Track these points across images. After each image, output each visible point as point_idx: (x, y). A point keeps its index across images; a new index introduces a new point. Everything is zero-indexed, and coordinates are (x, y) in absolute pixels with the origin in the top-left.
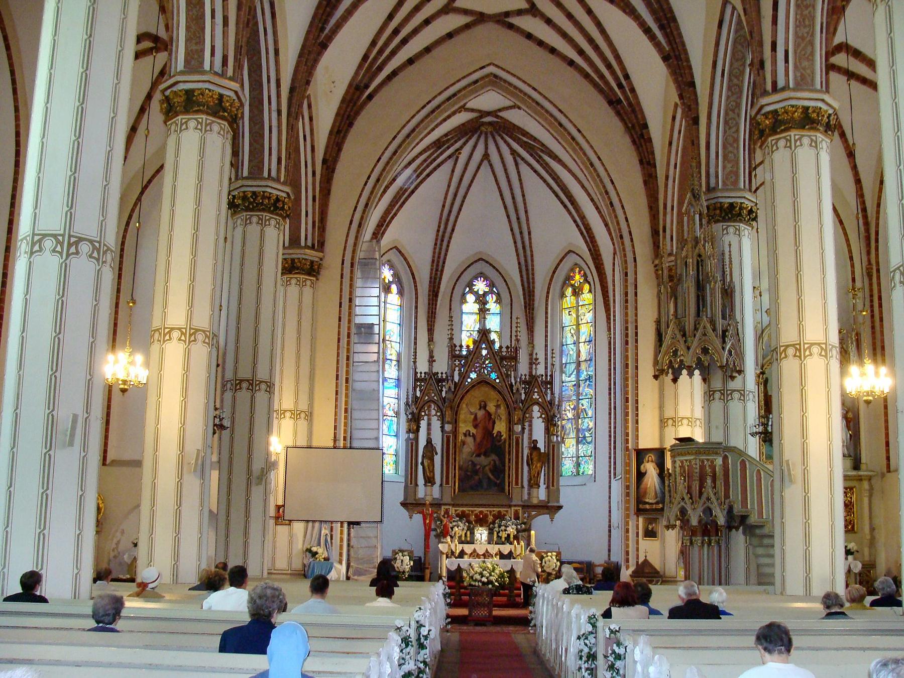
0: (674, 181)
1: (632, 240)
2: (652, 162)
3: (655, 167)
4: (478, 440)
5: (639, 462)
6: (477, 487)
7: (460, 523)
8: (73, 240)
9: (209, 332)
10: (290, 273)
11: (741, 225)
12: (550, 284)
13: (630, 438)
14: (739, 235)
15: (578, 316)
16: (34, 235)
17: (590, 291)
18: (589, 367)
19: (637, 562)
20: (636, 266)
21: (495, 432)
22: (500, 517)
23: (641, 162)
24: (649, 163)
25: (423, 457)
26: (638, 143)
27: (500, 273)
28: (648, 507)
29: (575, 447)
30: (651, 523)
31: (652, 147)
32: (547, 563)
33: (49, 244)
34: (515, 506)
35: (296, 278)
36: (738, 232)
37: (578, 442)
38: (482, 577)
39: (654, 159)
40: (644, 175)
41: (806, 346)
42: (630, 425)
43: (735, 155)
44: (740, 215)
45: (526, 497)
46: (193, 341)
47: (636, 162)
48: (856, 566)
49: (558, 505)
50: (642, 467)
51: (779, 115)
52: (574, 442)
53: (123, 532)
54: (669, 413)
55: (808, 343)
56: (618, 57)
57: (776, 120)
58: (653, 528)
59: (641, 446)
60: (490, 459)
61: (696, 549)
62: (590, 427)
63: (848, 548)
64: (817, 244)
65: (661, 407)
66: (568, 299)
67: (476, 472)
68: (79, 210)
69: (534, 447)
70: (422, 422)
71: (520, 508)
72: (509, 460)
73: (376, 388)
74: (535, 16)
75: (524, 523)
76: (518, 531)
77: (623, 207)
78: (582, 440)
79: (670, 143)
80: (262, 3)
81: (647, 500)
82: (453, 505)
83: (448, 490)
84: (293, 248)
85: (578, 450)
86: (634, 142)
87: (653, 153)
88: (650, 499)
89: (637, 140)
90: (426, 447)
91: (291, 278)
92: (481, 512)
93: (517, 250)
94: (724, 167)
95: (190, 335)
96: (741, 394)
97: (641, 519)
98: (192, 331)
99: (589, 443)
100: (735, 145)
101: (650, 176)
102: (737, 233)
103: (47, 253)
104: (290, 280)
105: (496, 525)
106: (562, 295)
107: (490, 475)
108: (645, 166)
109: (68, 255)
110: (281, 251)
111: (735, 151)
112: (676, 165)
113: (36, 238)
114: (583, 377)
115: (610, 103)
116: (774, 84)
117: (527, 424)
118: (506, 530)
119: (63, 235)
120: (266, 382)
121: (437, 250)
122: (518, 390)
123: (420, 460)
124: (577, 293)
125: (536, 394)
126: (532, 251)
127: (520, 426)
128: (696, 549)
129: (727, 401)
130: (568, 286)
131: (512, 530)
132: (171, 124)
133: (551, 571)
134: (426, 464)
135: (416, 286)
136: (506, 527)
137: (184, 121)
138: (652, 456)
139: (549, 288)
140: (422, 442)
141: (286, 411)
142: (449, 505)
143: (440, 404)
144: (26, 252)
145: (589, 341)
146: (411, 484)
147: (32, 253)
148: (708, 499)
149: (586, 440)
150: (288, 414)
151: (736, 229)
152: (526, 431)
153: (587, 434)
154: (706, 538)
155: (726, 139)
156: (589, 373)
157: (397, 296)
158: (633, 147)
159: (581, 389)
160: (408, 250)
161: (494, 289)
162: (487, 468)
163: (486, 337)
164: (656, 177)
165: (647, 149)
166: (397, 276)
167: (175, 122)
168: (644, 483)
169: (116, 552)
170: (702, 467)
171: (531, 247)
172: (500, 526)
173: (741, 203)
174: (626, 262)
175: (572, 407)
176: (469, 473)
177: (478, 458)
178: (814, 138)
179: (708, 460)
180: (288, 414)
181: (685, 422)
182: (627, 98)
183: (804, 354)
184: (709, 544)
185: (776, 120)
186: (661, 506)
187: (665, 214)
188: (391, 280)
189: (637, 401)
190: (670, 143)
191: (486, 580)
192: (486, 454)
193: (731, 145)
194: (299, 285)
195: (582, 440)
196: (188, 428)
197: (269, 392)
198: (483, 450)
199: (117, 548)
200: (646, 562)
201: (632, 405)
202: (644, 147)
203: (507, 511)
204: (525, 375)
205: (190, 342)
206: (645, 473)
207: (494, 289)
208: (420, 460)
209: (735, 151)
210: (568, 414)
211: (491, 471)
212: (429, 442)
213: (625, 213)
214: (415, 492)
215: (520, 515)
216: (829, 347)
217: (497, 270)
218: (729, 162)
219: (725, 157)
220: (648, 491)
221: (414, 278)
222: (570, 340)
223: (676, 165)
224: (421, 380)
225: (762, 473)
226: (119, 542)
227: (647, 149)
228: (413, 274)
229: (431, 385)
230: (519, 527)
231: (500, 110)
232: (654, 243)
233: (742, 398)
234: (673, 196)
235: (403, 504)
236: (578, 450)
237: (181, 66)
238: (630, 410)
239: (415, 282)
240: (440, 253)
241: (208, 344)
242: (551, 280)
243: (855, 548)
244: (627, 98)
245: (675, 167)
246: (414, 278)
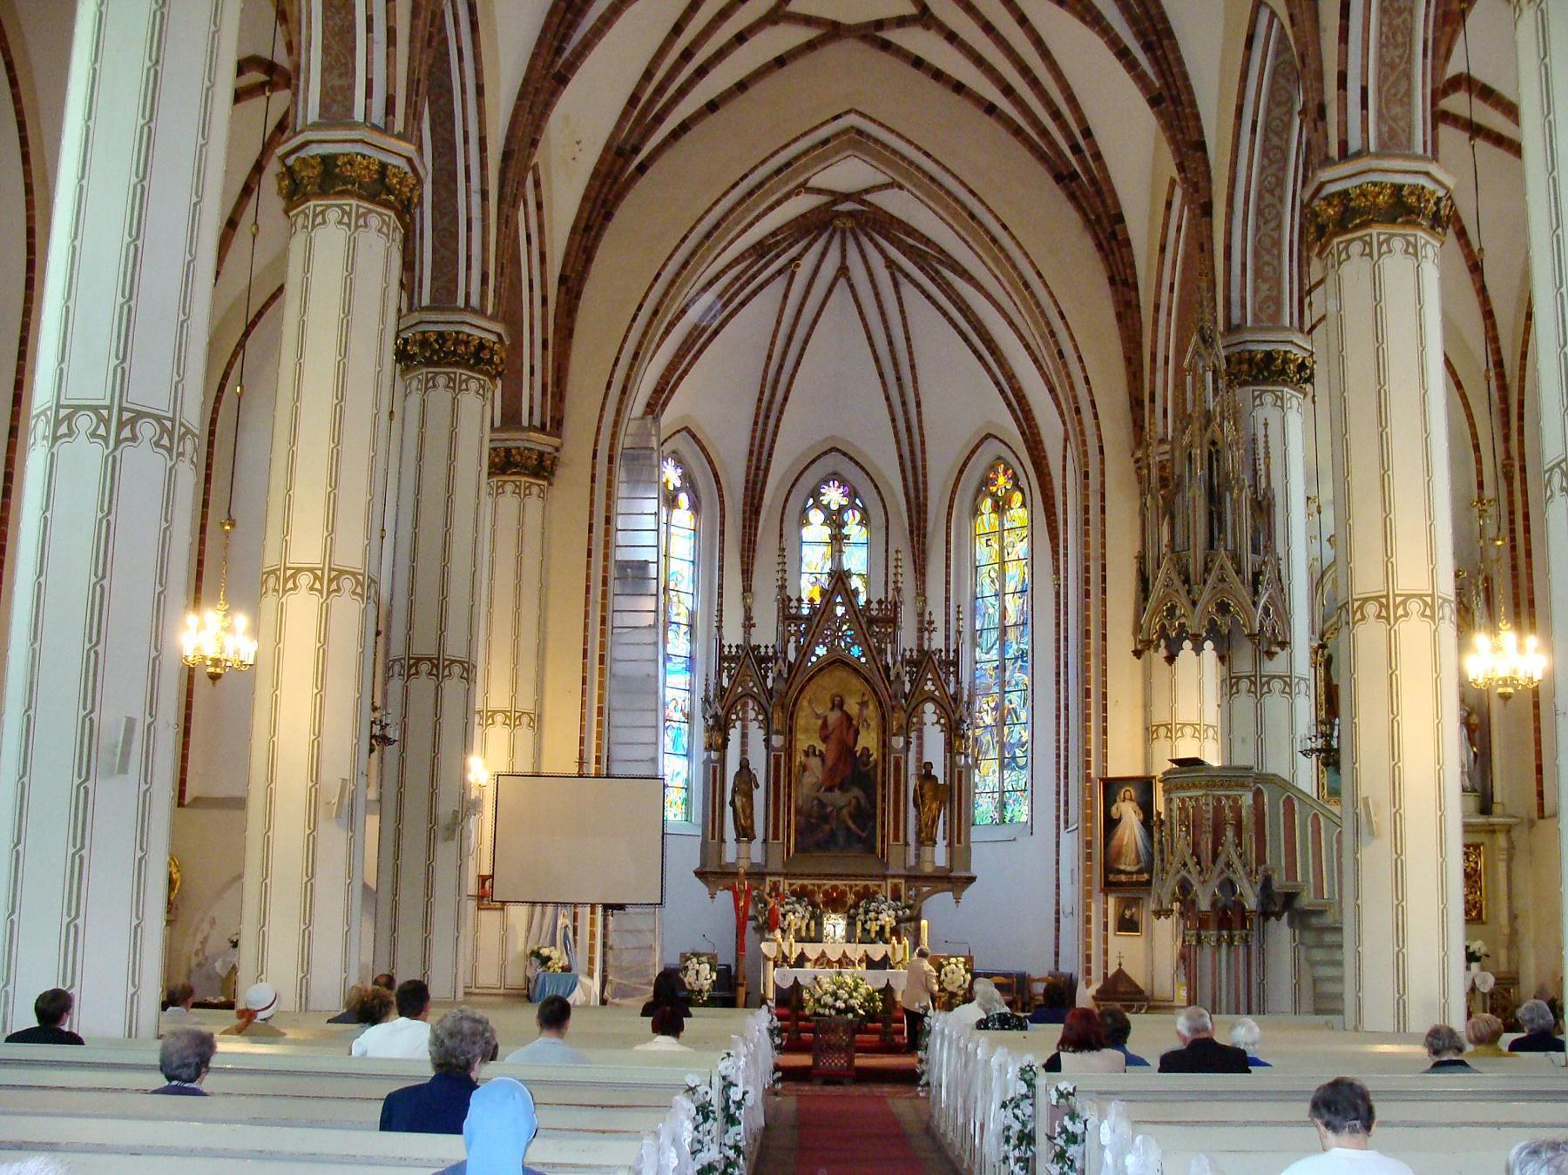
0: (1169, 314)
1: (1096, 416)
2: (1130, 281)
3: (1136, 289)
4: (829, 762)
5: (1109, 801)
6: (827, 844)
7: (797, 906)
8: (126, 415)
9: (363, 575)
10: (504, 473)
11: (1286, 389)
12: (954, 492)
13: (1093, 759)
14: (1282, 408)
15: (1002, 548)
16: (59, 406)
17: (1024, 505)
18: (1022, 636)
19: (1106, 974)
20: (1103, 462)
21: (858, 748)
22: (867, 895)
23: (1112, 280)
24: (1125, 283)
25: (734, 791)
26: (1106, 247)
27: (867, 474)
28: (1123, 878)
29: (997, 774)
30: (1129, 907)
31: (1131, 255)
32: (949, 975)
33: (84, 422)
34: (894, 876)
36: (1280, 403)
37: (1002, 767)
38: (836, 1000)
39: (1135, 275)
40: (1117, 303)
41: (1398, 600)
42: (1093, 736)
43: (1274, 269)
44: (1283, 372)
45: (912, 861)
46: (334, 591)
47: (1103, 280)
48: (1485, 981)
49: (967, 875)
50: (1114, 809)
51: (1351, 199)
52: (995, 765)
53: (213, 922)
54: (1160, 716)
55: (1401, 595)
56: (1071, 99)
57: (1346, 208)
58: (1132, 915)
59: (1112, 773)
60: (850, 795)
61: (1207, 951)
62: (1024, 740)
63: (1471, 950)
64: (1418, 423)
65: (1147, 706)
66: (985, 517)
68: (137, 364)
70: (732, 731)
71: (903, 881)
72: (884, 797)
73: (652, 673)
74: (927, 27)
75: (910, 907)
76: (899, 920)
77: (1080, 358)
78: (1009, 763)
79: (1163, 249)
80: (454, 6)
81: (1122, 867)
82: (786, 876)
83: (777, 848)
85: (1002, 780)
86: (1099, 246)
87: (1132, 265)
88: (1127, 864)
89: (1105, 243)
90: (738, 774)
91: (505, 482)
92: (834, 888)
93: (896, 434)
94: (1256, 290)
95: (330, 581)
96: (1285, 682)
97: (1111, 900)
98: (334, 574)
99: (1022, 768)
100: (1276, 252)
101: (1128, 304)
102: (1279, 403)
103: (82, 439)
105: (861, 910)
106: (976, 512)
107: (850, 823)
109: (118, 442)
110: (487, 436)
112: (1172, 285)
113: (63, 413)
114: (1011, 653)
115: (1059, 178)
116: (1343, 145)
117: (913, 735)
118: (877, 919)
119: (109, 408)
120: (461, 663)
121: (758, 434)
123: (728, 798)
124: (1000, 507)
125: (929, 683)
126: (922, 435)
127: (902, 739)
128: (1207, 951)
129: (1262, 695)
130: (986, 496)
131: (887, 919)
132: (297, 215)
133: (955, 990)
134: (739, 804)
135: (721, 496)
136: (878, 913)
137: (319, 209)
138: (1130, 791)
139: (952, 500)
140: (732, 767)
142: (779, 875)
143: (764, 701)
144: (44, 438)
145: (1022, 592)
146: (713, 838)
147: (55, 439)
148: (1229, 865)
149: (1017, 763)
151: (1277, 396)
152: (913, 747)
153: (1018, 753)
154: (1225, 933)
155: (1260, 240)
156: (1022, 646)
157: (689, 513)
158: (1098, 256)
159: (1008, 674)
160: (707, 434)
161: (858, 501)
162: (845, 811)
163: (844, 583)
164: (1138, 306)
165: (1122, 258)
166: (688, 479)
167: (303, 211)
168: (1117, 837)
169: (201, 957)
170: (1218, 810)
171: (921, 428)
172: (866, 912)
173: (1286, 352)
175: (992, 705)
176: (813, 820)
177: (829, 794)
178: (1412, 239)
179: (1227, 797)
181: (1188, 731)
182: (1087, 170)
183: (1395, 613)
185: (1346, 208)
186: (1146, 876)
187: (1153, 372)
188: (678, 485)
189: (1105, 696)
190: (1163, 249)
192: (843, 787)
193: (1269, 252)
194: (519, 494)
195: (1009, 763)
196: (327, 741)
197: (467, 680)
198: (838, 780)
199: (203, 949)
200: (1120, 973)
201: (1096, 702)
202: (1117, 254)
203: (879, 886)
204: (911, 650)
205: (329, 593)
206: (1120, 820)
207: (858, 501)
208: (728, 798)
209: (1276, 262)
210: (985, 717)
211: (851, 816)
212: (744, 765)
213: (1084, 369)
214: (720, 853)
215: (903, 893)
216: (1438, 602)
217: (862, 468)
218: (1265, 280)
219: (1258, 272)
220: (1124, 850)
221: (718, 482)
222: (988, 590)
223: (1172, 285)
224: (730, 659)
225: (1322, 819)
226: (206, 939)
227: (1122, 258)
228: (716, 475)
229: (748, 666)
230: (900, 913)
231: (867, 191)
232: (1135, 421)
233: (1287, 690)
234: (1168, 340)
235: (700, 874)
236: (1002, 780)
237: (313, 114)
238: (1092, 711)
239: (720, 489)
240: (763, 439)
241: (361, 596)
242: (956, 485)
243: (1483, 950)
244: (1087, 170)
245: (1172, 290)
246: (718, 482)
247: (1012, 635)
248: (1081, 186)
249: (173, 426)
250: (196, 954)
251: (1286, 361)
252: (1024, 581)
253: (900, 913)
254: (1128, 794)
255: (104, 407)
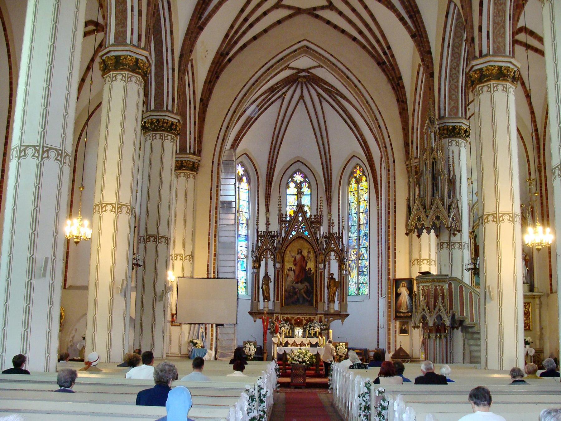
0: (418, 113)
1: (392, 149)
2: (404, 101)
3: (406, 103)
4: (297, 273)
5: (397, 287)
6: (296, 302)
7: (285, 325)
8: (45, 149)
9: (130, 206)
10: (180, 170)
11: (460, 139)
12: (341, 176)
13: (391, 272)
14: (459, 146)
15: (358, 196)
16: (21, 146)
17: (366, 181)
19: (396, 349)
20: (394, 165)
21: (307, 268)
22: (310, 321)
23: (398, 100)
24: (402, 101)
25: (263, 284)
26: (396, 88)
27: (310, 170)
28: (402, 315)
29: (357, 277)
30: (404, 325)
31: (405, 91)
32: (340, 349)
33: (30, 151)
34: (320, 314)
35: (184, 173)
36: (458, 144)
37: (359, 275)
38: (299, 358)
39: (406, 99)
40: (400, 108)
41: (500, 215)
42: (391, 264)
43: (456, 96)
44: (459, 133)
45: (326, 309)
46: (120, 212)
47: (395, 100)
48: (531, 352)
50: (398, 290)
52: (356, 274)
53: (76, 330)
54: (415, 256)
58: (405, 328)
59: (398, 277)
60: (304, 285)
61: (432, 341)
62: (366, 265)
63: (526, 340)
64: (507, 151)
65: (410, 253)
66: (352, 185)
67: (295, 293)
68: (49, 131)
69: (331, 278)
70: (262, 262)
71: (323, 316)
72: (316, 285)
73: (233, 241)
75: (325, 325)
76: (322, 330)
77: (386, 128)
78: (361, 274)
79: (416, 89)
80: (162, 2)
81: (402, 311)
82: (281, 314)
83: (278, 304)
84: (182, 154)
85: (358, 279)
86: (393, 88)
87: (405, 95)
88: (403, 310)
89: (395, 87)
90: (264, 277)
91: (181, 173)
92: (299, 318)
93: (321, 155)
94: (449, 104)
95: (118, 208)
96: (460, 244)
97: (398, 323)
98: (119, 206)
99: (365, 275)
100: (456, 90)
101: (403, 109)
102: (458, 144)
103: (29, 157)
104: (180, 174)
105: (308, 326)
106: (349, 183)
107: (304, 295)
108: (401, 103)
109: (42, 158)
110: (174, 156)
111: (456, 94)
112: (419, 102)
113: (23, 148)
114: (362, 234)
115: (379, 64)
117: (327, 263)
118: (314, 329)
119: (39, 146)
120: (165, 237)
121: (271, 155)
122: (321, 242)
123: (261, 286)
124: (358, 182)
125: (333, 245)
126: (330, 156)
127: (323, 265)
128: (432, 341)
129: (451, 249)
130: (353, 178)
131: (317, 329)
132: (106, 77)
133: (342, 355)
134: (264, 288)
135: (258, 178)
136: (314, 327)
137: (114, 75)
138: (404, 283)
139: (341, 179)
140: (262, 275)
141: (177, 255)
142: (279, 313)
143: (273, 251)
144: (16, 157)
145: (366, 212)
146: (255, 300)
147: (20, 157)
148: (440, 310)
149: (364, 273)
150: (179, 257)
151: (457, 142)
152: (327, 268)
153: (364, 270)
154: (438, 334)
155: (451, 86)
156: (366, 232)
157: (247, 184)
158: (393, 92)
159: (360, 241)
160: (253, 155)
161: (307, 180)
162: (302, 291)
163: (302, 209)
164: (407, 110)
165: (401, 93)
166: (246, 172)
167: (108, 76)
168: (399, 300)
169: (72, 343)
170: (436, 290)
171: (329, 153)
172: (310, 327)
173: (460, 126)
174: (388, 163)
175: (355, 253)
176: (291, 294)
177: (297, 285)
178: (505, 86)
179: (439, 286)
180: (179, 257)
181: (425, 262)
182: (389, 61)
183: (499, 220)
184: (440, 338)
186: (410, 314)
187: (413, 133)
188: (243, 174)
189: (395, 249)
190: (416, 89)
191: (301, 360)
192: (301, 282)
193: (454, 90)
195: (361, 274)
196: (117, 265)
197: (167, 243)
198: (300, 280)
199: (73, 340)
200: (401, 349)
201: (392, 252)
202: (400, 91)
203: (315, 317)
204: (326, 233)
205: (118, 212)
206: (401, 294)
207: (307, 180)
208: (261, 286)
209: (456, 94)
210: (352, 257)
211: (305, 292)
212: (266, 274)
213: (388, 132)
214: (258, 306)
215: (323, 320)
216: (515, 216)
217: (308, 168)
218: (453, 100)
219: (450, 97)
220: (402, 305)
221: (257, 173)
222: (354, 211)
223: (419, 102)
224: (261, 236)
225: (473, 294)
226: (74, 336)
227: (401, 93)
228: (256, 170)
230: (322, 327)
232: (406, 151)
233: (461, 247)
234: (418, 122)
235: (250, 313)
236: (358, 279)
237: (112, 41)
238: (391, 255)
239: (257, 175)
240: (273, 157)
241: (129, 213)
242: (342, 174)
243: (531, 340)
244: (389, 61)
245: (419, 104)
246: (257, 173)
247: (362, 227)
248: (387, 67)
249: (62, 153)
250: (70, 342)
251: (460, 129)
252: (366, 208)
253: (322, 327)
254: (403, 284)
255: (37, 146)
